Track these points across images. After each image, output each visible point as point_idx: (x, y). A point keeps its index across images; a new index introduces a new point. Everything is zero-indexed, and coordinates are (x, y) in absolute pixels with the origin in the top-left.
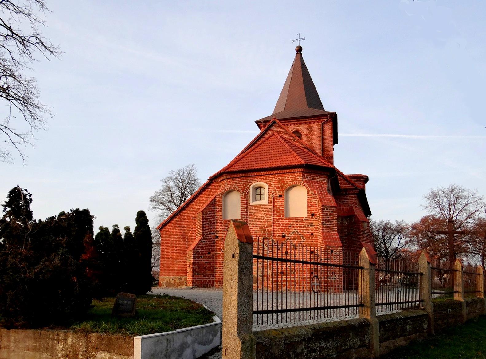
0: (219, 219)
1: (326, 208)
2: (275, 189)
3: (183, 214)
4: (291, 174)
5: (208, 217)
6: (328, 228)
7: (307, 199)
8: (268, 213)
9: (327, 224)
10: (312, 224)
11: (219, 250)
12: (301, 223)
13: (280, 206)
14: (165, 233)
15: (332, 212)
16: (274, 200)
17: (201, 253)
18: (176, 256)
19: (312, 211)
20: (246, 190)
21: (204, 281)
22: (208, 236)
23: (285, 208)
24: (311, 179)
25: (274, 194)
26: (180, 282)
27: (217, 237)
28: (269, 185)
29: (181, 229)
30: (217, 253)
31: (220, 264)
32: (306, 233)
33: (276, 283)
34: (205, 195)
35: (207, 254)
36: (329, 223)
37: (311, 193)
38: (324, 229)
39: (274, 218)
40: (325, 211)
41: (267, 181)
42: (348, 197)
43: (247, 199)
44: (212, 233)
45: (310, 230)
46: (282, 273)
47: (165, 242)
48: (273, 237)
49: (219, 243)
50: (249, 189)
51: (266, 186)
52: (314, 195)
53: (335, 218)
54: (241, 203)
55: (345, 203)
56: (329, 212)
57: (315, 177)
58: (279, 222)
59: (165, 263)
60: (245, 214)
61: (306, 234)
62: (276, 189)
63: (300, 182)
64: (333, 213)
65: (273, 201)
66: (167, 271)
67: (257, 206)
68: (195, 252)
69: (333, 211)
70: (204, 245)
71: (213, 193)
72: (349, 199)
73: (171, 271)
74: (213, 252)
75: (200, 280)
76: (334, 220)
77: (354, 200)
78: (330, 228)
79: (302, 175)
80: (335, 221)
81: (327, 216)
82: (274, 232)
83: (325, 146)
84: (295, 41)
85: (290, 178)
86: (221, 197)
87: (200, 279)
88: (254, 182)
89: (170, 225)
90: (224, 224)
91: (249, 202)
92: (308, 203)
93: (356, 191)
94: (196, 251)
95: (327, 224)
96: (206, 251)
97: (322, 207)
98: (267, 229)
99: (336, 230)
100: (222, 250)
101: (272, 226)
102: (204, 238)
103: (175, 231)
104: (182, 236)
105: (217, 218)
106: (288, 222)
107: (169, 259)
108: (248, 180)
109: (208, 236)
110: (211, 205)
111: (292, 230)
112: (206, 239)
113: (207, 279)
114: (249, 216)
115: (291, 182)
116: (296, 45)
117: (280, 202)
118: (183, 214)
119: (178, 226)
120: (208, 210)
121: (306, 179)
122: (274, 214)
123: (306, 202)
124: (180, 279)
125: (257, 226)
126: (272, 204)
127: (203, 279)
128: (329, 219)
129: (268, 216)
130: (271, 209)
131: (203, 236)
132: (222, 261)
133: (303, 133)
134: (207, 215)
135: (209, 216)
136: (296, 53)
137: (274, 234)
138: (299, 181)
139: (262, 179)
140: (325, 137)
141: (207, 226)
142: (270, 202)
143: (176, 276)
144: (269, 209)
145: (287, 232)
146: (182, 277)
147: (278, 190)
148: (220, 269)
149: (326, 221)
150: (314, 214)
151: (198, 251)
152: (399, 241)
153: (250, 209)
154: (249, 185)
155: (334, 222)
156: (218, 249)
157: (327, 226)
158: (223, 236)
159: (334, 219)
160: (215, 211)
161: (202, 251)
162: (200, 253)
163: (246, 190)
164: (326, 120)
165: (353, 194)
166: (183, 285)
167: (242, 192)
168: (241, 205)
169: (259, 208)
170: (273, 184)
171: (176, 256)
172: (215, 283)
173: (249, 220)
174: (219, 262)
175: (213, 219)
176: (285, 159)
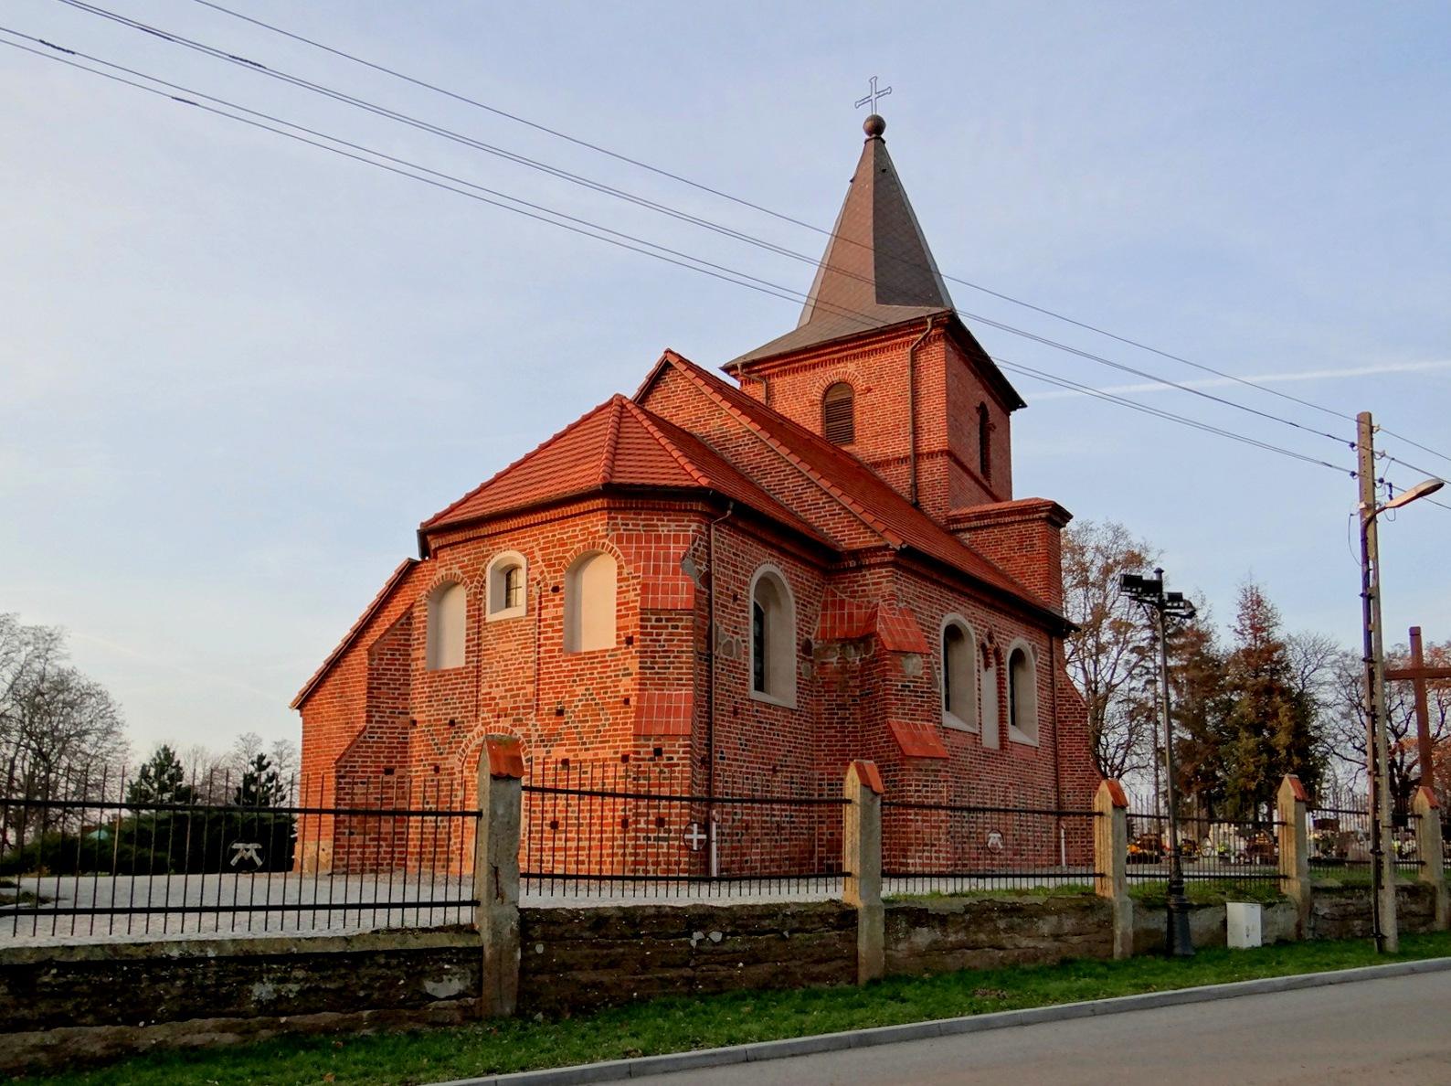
0: (417, 670)
1: (654, 618)
5: (387, 664)
6: (659, 679)
7: (618, 593)
9: (656, 666)
10: (628, 669)
12: (602, 667)
13: (553, 618)
15: (677, 627)
16: (540, 603)
17: (363, 772)
19: (627, 627)
20: (478, 578)
22: (386, 722)
23: (571, 623)
24: (641, 528)
25: (542, 585)
27: (414, 723)
28: (530, 555)
30: (411, 771)
32: (612, 700)
33: (539, 857)
35: (381, 775)
36: (665, 663)
37: (625, 571)
38: (645, 684)
39: (539, 659)
40: (652, 627)
41: (526, 546)
42: (868, 577)
44: (400, 713)
45: (622, 690)
46: (554, 825)
48: (536, 715)
51: (521, 560)
52: (633, 578)
53: (687, 646)
54: (468, 617)
55: (860, 597)
56: (666, 627)
57: (655, 522)
60: (474, 651)
61: (611, 700)
62: (545, 570)
63: (602, 541)
64: (680, 630)
65: (537, 606)
68: (343, 770)
69: (680, 624)
70: (372, 747)
72: (870, 581)
74: (400, 767)
76: (682, 652)
77: (885, 584)
78: (668, 679)
79: (609, 518)
80: (687, 658)
81: (659, 641)
82: (538, 700)
83: (922, 419)
84: (863, 102)
85: (581, 530)
86: (425, 605)
88: (497, 551)
92: (618, 605)
93: (885, 555)
94: (346, 767)
95: (656, 666)
96: (379, 767)
97: (641, 614)
98: (522, 691)
99: (689, 685)
101: (533, 682)
102: (371, 727)
106: (570, 668)
109: (386, 722)
110: (397, 630)
111: (580, 690)
112: (379, 730)
115: (581, 545)
116: (866, 113)
117: (555, 606)
120: (388, 644)
121: (622, 532)
122: (539, 646)
123: (615, 602)
126: (536, 617)
128: (664, 652)
130: (531, 630)
131: (371, 722)
134: (382, 659)
135: (393, 661)
136: (867, 137)
137: (538, 705)
138: (601, 537)
140: (923, 391)
141: (384, 693)
142: (530, 610)
145: (567, 699)
147: (549, 572)
149: (655, 657)
150: (632, 638)
151: (351, 767)
152: (1443, 715)
155: (684, 659)
157: (658, 673)
159: (685, 649)
160: (410, 645)
161: (367, 767)
162: (357, 772)
163: (478, 578)
164: (920, 336)
165: (882, 565)
168: (467, 623)
170: (538, 554)
175: (404, 670)
176: (570, 477)
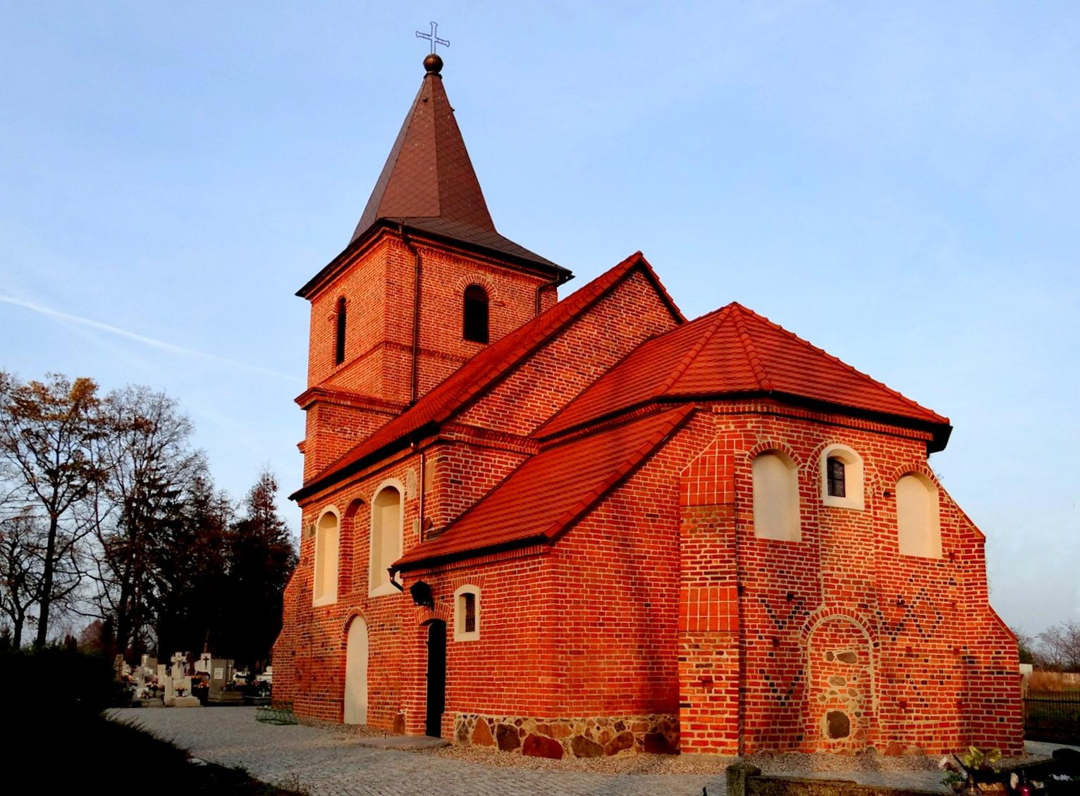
2: (877, 472)
3: (620, 496)
4: (906, 442)
8: (866, 536)
11: (749, 631)
14: (567, 557)
18: (601, 644)
26: (619, 738)
29: (616, 550)
31: (755, 677)
34: (679, 448)
43: (816, 487)
47: (566, 591)
49: (748, 611)
50: (818, 459)
58: (889, 566)
59: (568, 670)
60: (811, 530)
62: (879, 475)
66: (573, 698)
67: (840, 512)
71: (699, 445)
73: (589, 697)
89: (581, 530)
90: (761, 550)
91: (819, 496)
100: (757, 632)
103: (600, 554)
104: (619, 572)
105: (740, 530)
106: (906, 568)
107: (579, 653)
108: (815, 433)
114: (821, 536)
115: (907, 464)
116: (424, 51)
118: (620, 496)
119: (607, 538)
124: (620, 726)
125: (842, 568)
129: (866, 545)
132: (758, 669)
133: (495, 295)
139: (847, 439)
143: (604, 715)
144: (866, 525)
145: (906, 594)
146: (627, 719)
148: (756, 694)
153: (823, 517)
154: (818, 447)
156: (746, 629)
158: (760, 588)
166: (630, 746)
167: (803, 464)
169: (843, 517)
171: (601, 644)
173: (822, 550)
174: (751, 671)
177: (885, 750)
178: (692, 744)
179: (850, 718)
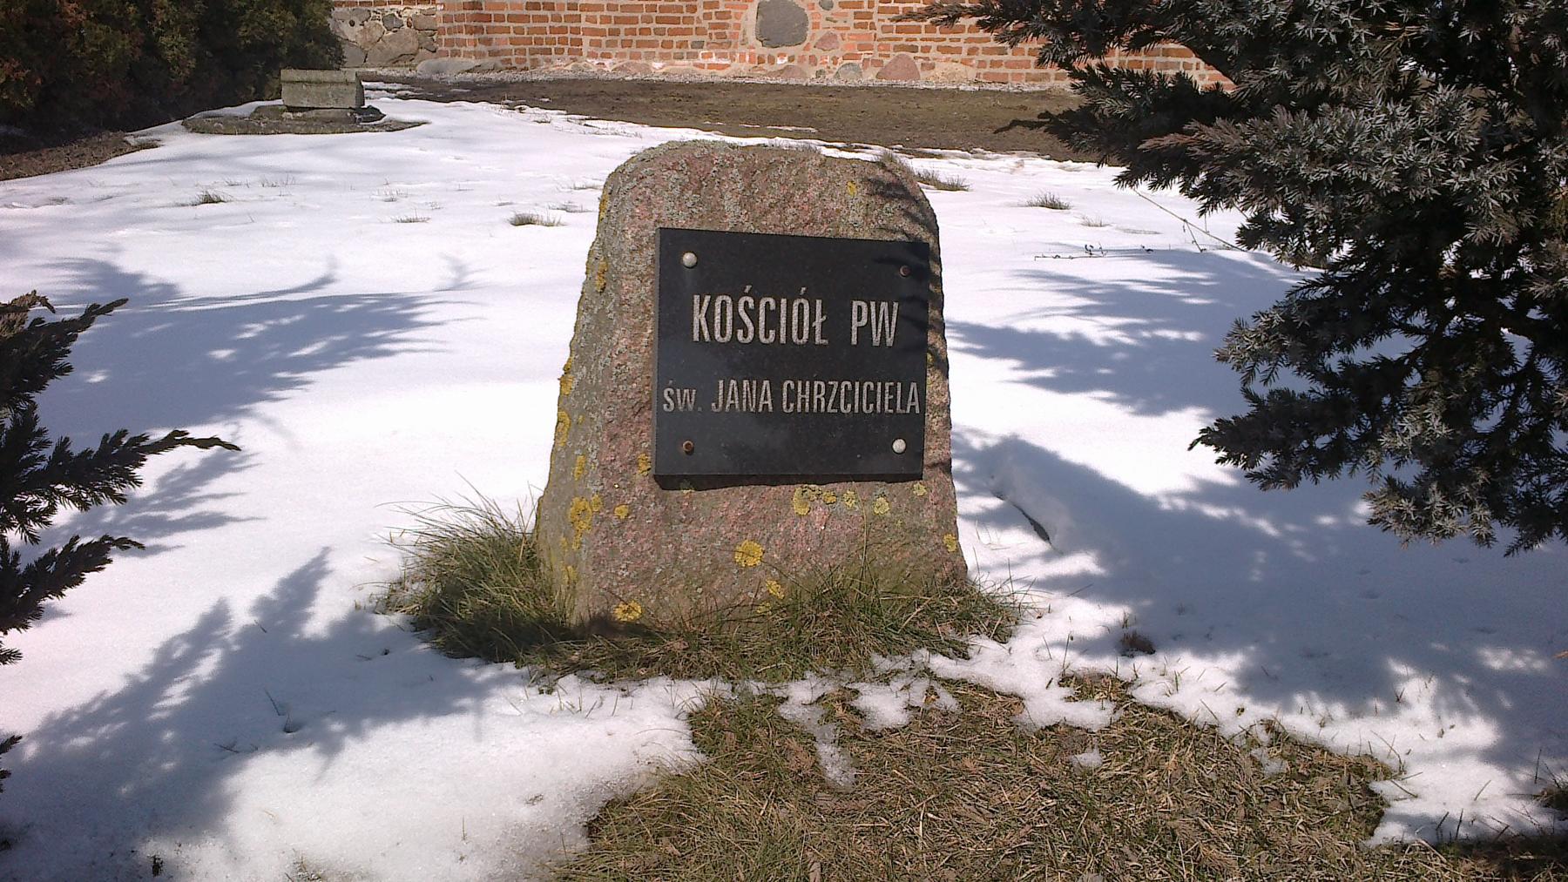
21: (532, 31)
75: (512, 25)
87: (511, 18)
113: (544, 19)
127: (524, 18)
172: (586, 40)
177: (878, 69)
178: (930, 47)
179: (808, 13)
